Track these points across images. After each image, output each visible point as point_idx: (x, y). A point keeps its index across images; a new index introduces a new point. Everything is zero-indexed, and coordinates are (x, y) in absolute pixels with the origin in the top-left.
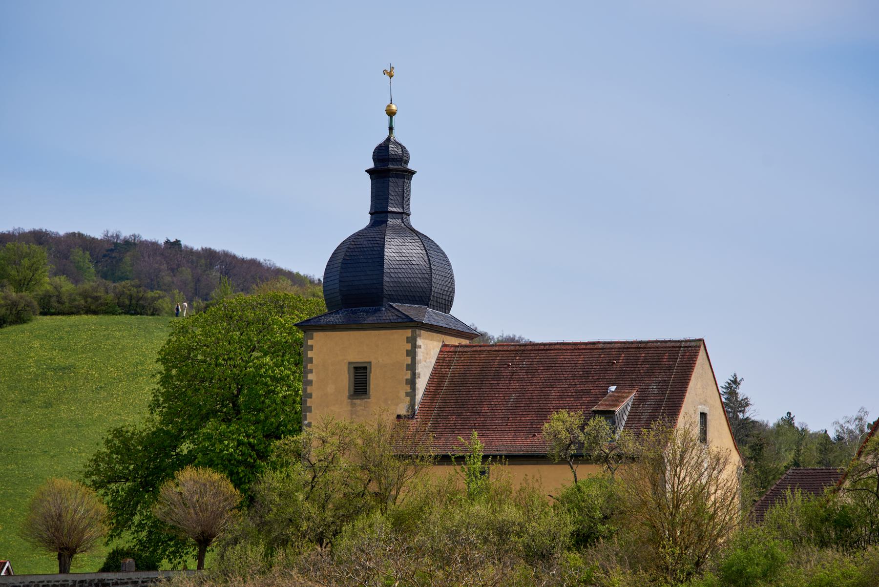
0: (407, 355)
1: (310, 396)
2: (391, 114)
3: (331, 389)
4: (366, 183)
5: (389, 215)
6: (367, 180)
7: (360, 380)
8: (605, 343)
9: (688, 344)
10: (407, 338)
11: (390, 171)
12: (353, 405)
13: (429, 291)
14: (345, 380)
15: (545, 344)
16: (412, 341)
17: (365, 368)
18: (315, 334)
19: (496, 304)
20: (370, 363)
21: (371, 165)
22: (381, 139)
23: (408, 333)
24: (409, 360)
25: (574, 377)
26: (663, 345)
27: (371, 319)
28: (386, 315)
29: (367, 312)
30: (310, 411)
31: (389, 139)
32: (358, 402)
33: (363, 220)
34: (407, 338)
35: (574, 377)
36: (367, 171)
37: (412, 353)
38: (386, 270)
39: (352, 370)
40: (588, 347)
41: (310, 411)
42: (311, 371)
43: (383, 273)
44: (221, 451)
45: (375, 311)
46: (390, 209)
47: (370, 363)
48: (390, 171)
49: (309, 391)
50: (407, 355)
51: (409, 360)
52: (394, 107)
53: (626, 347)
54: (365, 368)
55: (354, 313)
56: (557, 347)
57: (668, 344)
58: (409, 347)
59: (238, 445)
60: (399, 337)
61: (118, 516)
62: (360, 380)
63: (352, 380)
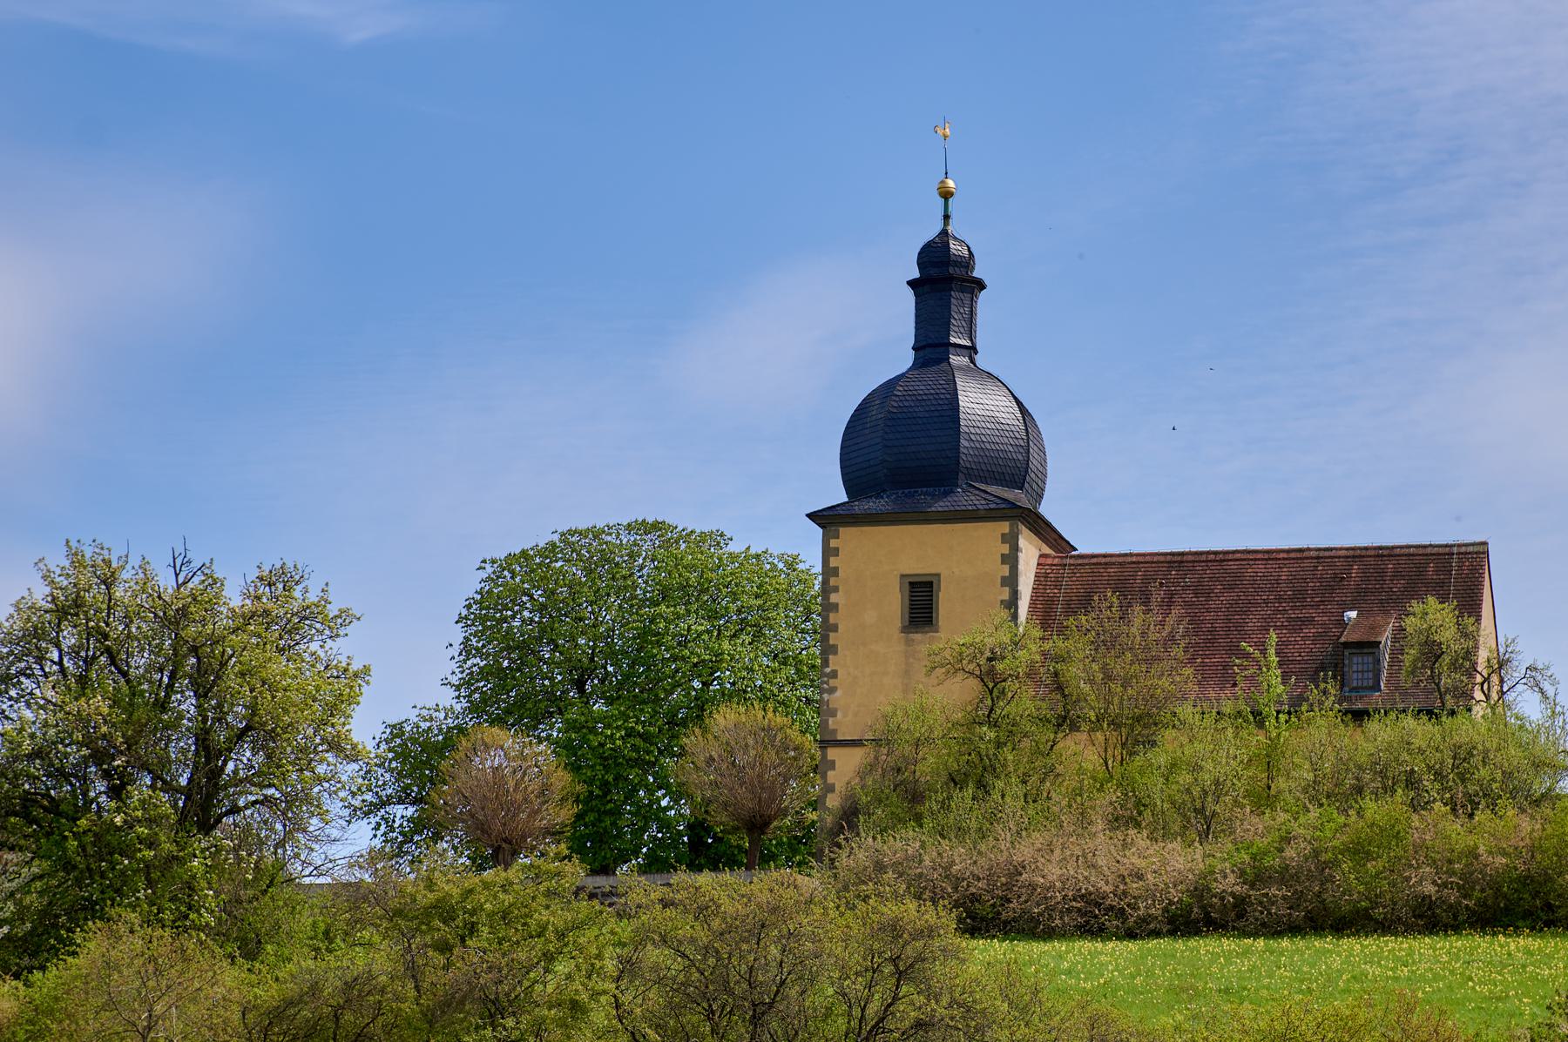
0: (1003, 562)
1: (835, 628)
2: (946, 195)
4: (907, 301)
5: (951, 349)
6: (910, 296)
7: (921, 601)
8: (1319, 550)
9: (1463, 549)
10: (1003, 535)
11: (944, 281)
12: (909, 642)
13: (1002, 483)
14: (895, 604)
15: (1216, 553)
16: (1012, 540)
17: (930, 584)
19: (1107, 502)
20: (938, 575)
21: (915, 274)
22: (931, 232)
23: (1005, 527)
25: (1279, 599)
26: (1421, 551)
27: (941, 506)
30: (836, 653)
31: (944, 233)
32: (918, 637)
33: (902, 359)
34: (1003, 535)
35: (1279, 599)
36: (910, 283)
37: (1011, 559)
38: (963, 429)
39: (907, 586)
40: (1293, 555)
41: (836, 653)
42: (836, 589)
45: (946, 494)
46: (953, 340)
47: (938, 575)
48: (944, 281)
49: (832, 621)
50: (1003, 562)
52: (951, 183)
53: (1357, 555)
54: (930, 584)
56: (1238, 556)
57: (1429, 550)
58: (1006, 549)
59: (628, 735)
60: (989, 535)
62: (921, 601)
63: (907, 602)
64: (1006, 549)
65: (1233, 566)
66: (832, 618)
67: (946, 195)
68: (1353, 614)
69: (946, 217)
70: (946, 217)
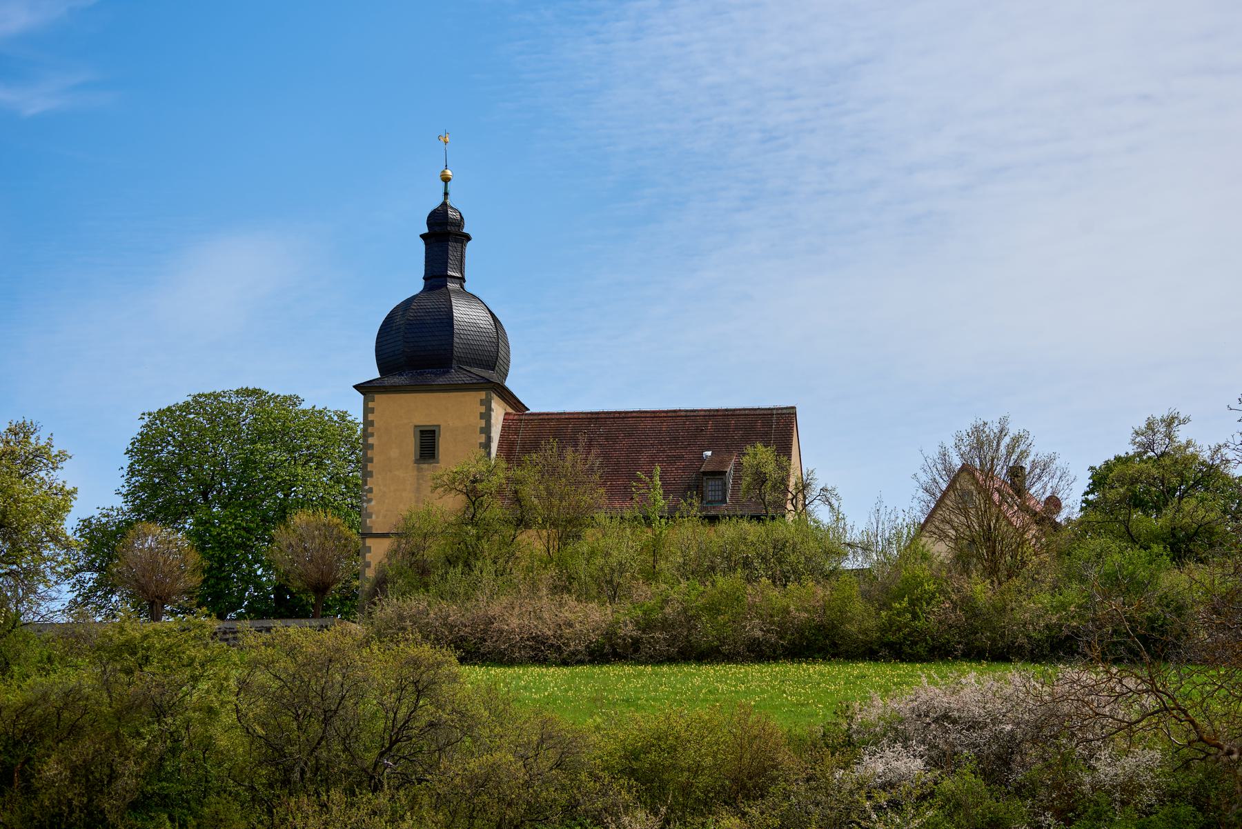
1: (371, 460)
2: (446, 180)
3: (394, 453)
6: (421, 245)
11: (444, 235)
12: (419, 470)
14: (411, 445)
17: (434, 431)
18: (377, 396)
19: (554, 375)
21: (426, 230)
24: (483, 423)
27: (441, 380)
28: (456, 376)
29: (436, 375)
30: (372, 476)
31: (444, 204)
32: (425, 466)
33: (413, 283)
37: (487, 416)
38: (456, 331)
41: (372, 476)
42: (372, 435)
43: (452, 333)
44: (219, 534)
45: (444, 373)
46: (449, 273)
48: (444, 235)
51: (483, 423)
52: (449, 172)
54: (434, 431)
55: (421, 374)
60: (471, 401)
61: (454, 544)
64: (483, 409)
65: (631, 421)
66: (370, 453)
67: (446, 180)
68: (709, 453)
69: (446, 194)
70: (446, 194)
